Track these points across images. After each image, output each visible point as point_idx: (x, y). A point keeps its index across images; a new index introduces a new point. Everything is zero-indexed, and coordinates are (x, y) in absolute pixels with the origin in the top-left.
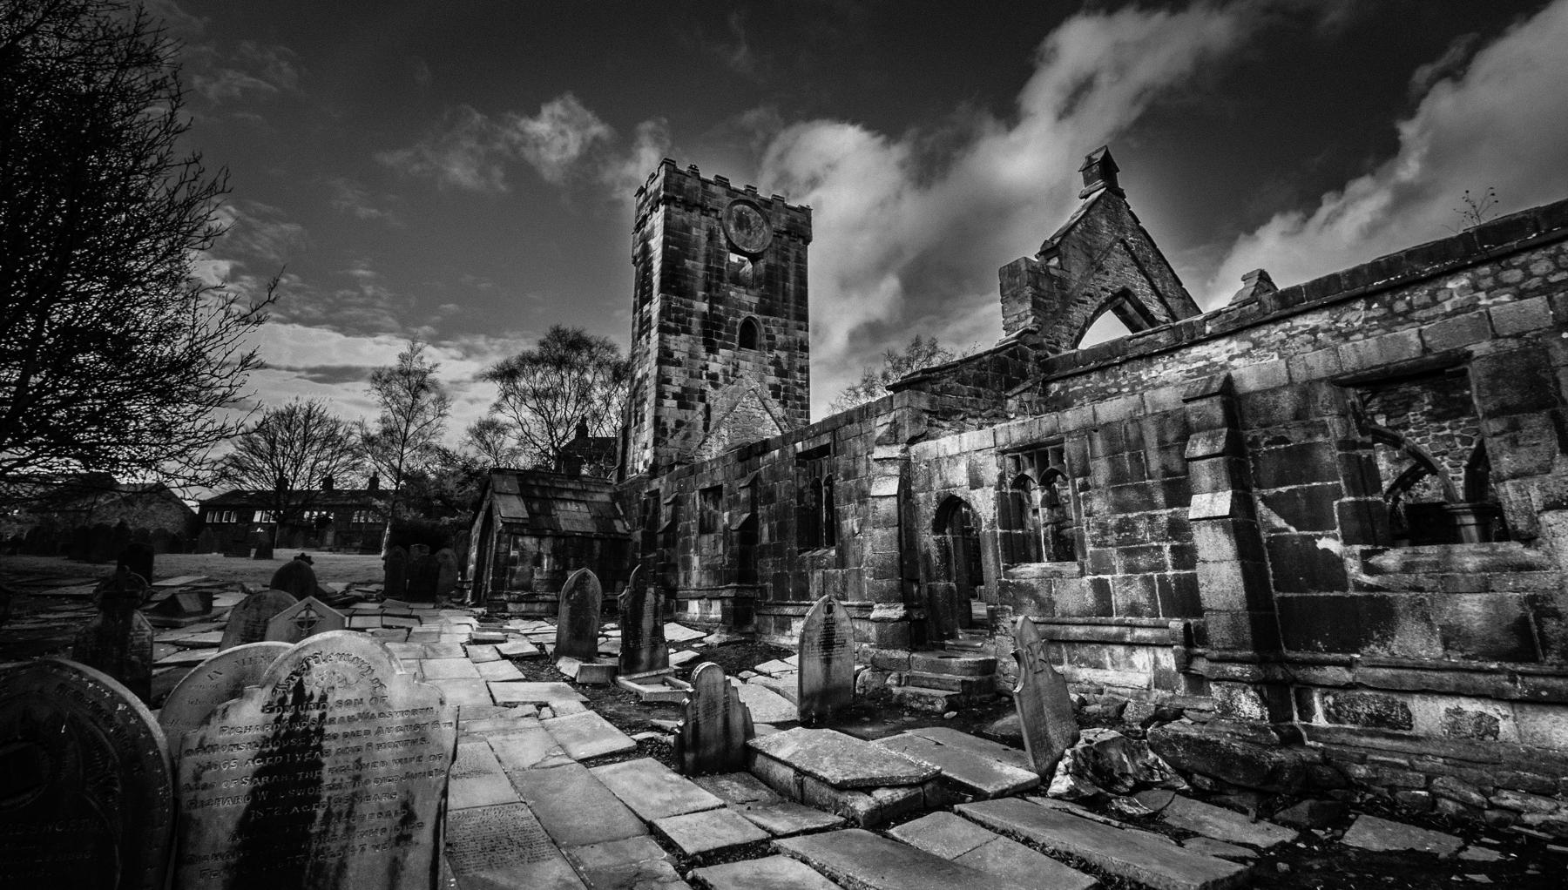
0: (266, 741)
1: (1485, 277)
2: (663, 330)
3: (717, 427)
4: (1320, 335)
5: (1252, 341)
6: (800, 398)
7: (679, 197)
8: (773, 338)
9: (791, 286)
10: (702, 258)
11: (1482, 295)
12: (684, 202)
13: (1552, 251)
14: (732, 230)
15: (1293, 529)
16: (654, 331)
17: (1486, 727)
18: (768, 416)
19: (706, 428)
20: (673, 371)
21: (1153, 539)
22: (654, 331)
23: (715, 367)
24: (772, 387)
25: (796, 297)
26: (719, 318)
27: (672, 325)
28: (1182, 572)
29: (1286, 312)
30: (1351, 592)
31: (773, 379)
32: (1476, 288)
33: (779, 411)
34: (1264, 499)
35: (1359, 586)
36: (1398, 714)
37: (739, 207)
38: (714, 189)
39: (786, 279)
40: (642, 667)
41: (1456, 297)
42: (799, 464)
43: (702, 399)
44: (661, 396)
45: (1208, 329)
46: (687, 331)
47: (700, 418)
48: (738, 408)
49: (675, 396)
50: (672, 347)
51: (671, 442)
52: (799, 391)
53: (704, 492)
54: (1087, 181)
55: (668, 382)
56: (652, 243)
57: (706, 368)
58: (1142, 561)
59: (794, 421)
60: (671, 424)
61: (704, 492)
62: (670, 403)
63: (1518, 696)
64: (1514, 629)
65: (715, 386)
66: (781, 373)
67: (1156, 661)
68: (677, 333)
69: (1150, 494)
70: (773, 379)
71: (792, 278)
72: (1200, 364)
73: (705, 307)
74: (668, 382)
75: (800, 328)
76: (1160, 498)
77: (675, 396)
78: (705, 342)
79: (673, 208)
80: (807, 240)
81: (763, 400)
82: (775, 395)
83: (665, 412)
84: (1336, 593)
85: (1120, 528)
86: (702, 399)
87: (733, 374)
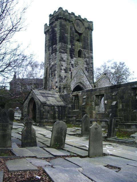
9: (89, 42)
14: (76, 27)
19: (71, 78)
24: (86, 68)
31: (85, 66)
33: (87, 74)
37: (76, 21)
39: (88, 40)
46: (66, 53)
49: (64, 70)
52: (91, 69)
53: (96, 96)
57: (71, 62)
61: (96, 96)
65: (73, 67)
70: (85, 66)
77: (64, 70)
82: (86, 70)
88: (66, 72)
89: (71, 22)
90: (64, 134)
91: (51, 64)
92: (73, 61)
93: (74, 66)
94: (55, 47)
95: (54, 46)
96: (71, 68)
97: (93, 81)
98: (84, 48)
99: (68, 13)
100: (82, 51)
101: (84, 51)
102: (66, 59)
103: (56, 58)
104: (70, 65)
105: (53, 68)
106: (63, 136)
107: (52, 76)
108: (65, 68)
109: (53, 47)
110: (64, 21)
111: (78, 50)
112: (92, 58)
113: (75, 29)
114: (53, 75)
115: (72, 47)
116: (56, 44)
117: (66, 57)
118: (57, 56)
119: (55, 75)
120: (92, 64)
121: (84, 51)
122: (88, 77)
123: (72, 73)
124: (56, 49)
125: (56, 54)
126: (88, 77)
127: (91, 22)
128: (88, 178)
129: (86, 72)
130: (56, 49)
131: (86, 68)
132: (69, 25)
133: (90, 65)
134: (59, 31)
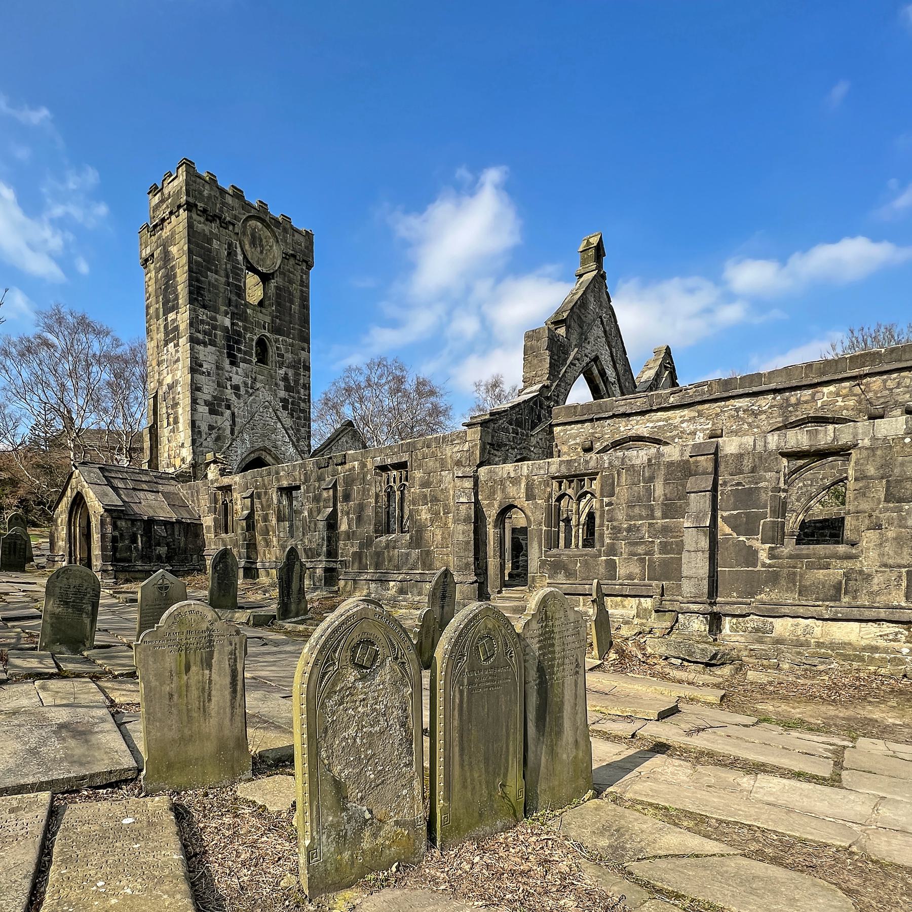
0: (540, 635)
1: (845, 388)
2: (193, 340)
3: (241, 432)
4: (741, 413)
5: (698, 412)
6: (303, 411)
7: (200, 205)
8: (282, 356)
9: (295, 307)
10: (222, 273)
11: (840, 399)
12: (205, 211)
13: (885, 377)
14: (247, 247)
15: (735, 535)
16: (183, 341)
17: (807, 631)
18: (279, 425)
19: (232, 433)
20: (202, 379)
21: (650, 537)
22: (183, 341)
23: (237, 380)
24: (284, 401)
25: (300, 318)
26: (239, 334)
27: (201, 336)
28: (664, 556)
29: (725, 395)
30: (759, 568)
31: (282, 394)
32: (838, 395)
33: (288, 422)
34: (722, 517)
35: (764, 565)
36: (769, 627)
37: (253, 223)
38: (229, 200)
39: (291, 302)
40: (291, 615)
41: (825, 398)
42: (376, 474)
43: (228, 407)
44: (194, 401)
45: (672, 399)
46: (213, 343)
47: (228, 424)
48: (257, 417)
49: (207, 403)
50: (201, 357)
51: (205, 443)
52: (302, 404)
53: (281, 489)
54: (584, 262)
55: (199, 389)
56: (174, 250)
57: (230, 379)
58: (640, 550)
59: (298, 430)
60: (204, 428)
61: (281, 489)
62: (203, 409)
63: (827, 617)
64: (834, 586)
65: (238, 396)
66: (288, 389)
67: (640, 603)
68: (205, 345)
69: (652, 511)
70: (282, 394)
71: (297, 301)
72: (661, 423)
73: (227, 322)
74: (199, 389)
75: (303, 349)
76: (658, 514)
77: (207, 403)
78: (231, 356)
79: (195, 216)
80: (309, 267)
81: (275, 411)
82: (285, 408)
83: (198, 417)
84: (750, 569)
85: (629, 530)
86: (228, 407)
87: (252, 389)
88: (212, 412)
89: (231, 228)
90: (90, 608)
91: (163, 380)
92: (237, 373)
93: (242, 391)
94: (174, 320)
95: (171, 316)
96: (234, 398)
97: (309, 446)
98: (277, 330)
99: (218, 187)
100: (270, 341)
101: (277, 341)
102: (214, 367)
103: (178, 360)
104: (229, 387)
105: (171, 396)
106: (87, 614)
107: (168, 424)
108: (209, 398)
109: (169, 319)
110: (202, 220)
111: (255, 338)
112: (307, 368)
113: (245, 257)
114: (171, 420)
115: (233, 324)
116: (175, 308)
117: (212, 358)
118: (180, 354)
119: (176, 422)
120: (307, 387)
121: (278, 344)
122: (291, 432)
123: (233, 414)
124: (177, 326)
125: (176, 345)
126: (291, 432)
127: (309, 236)
128: (576, 699)
129: (284, 414)
130: (176, 328)
131: (284, 401)
132: (223, 239)
133: (299, 393)
134: (185, 259)
